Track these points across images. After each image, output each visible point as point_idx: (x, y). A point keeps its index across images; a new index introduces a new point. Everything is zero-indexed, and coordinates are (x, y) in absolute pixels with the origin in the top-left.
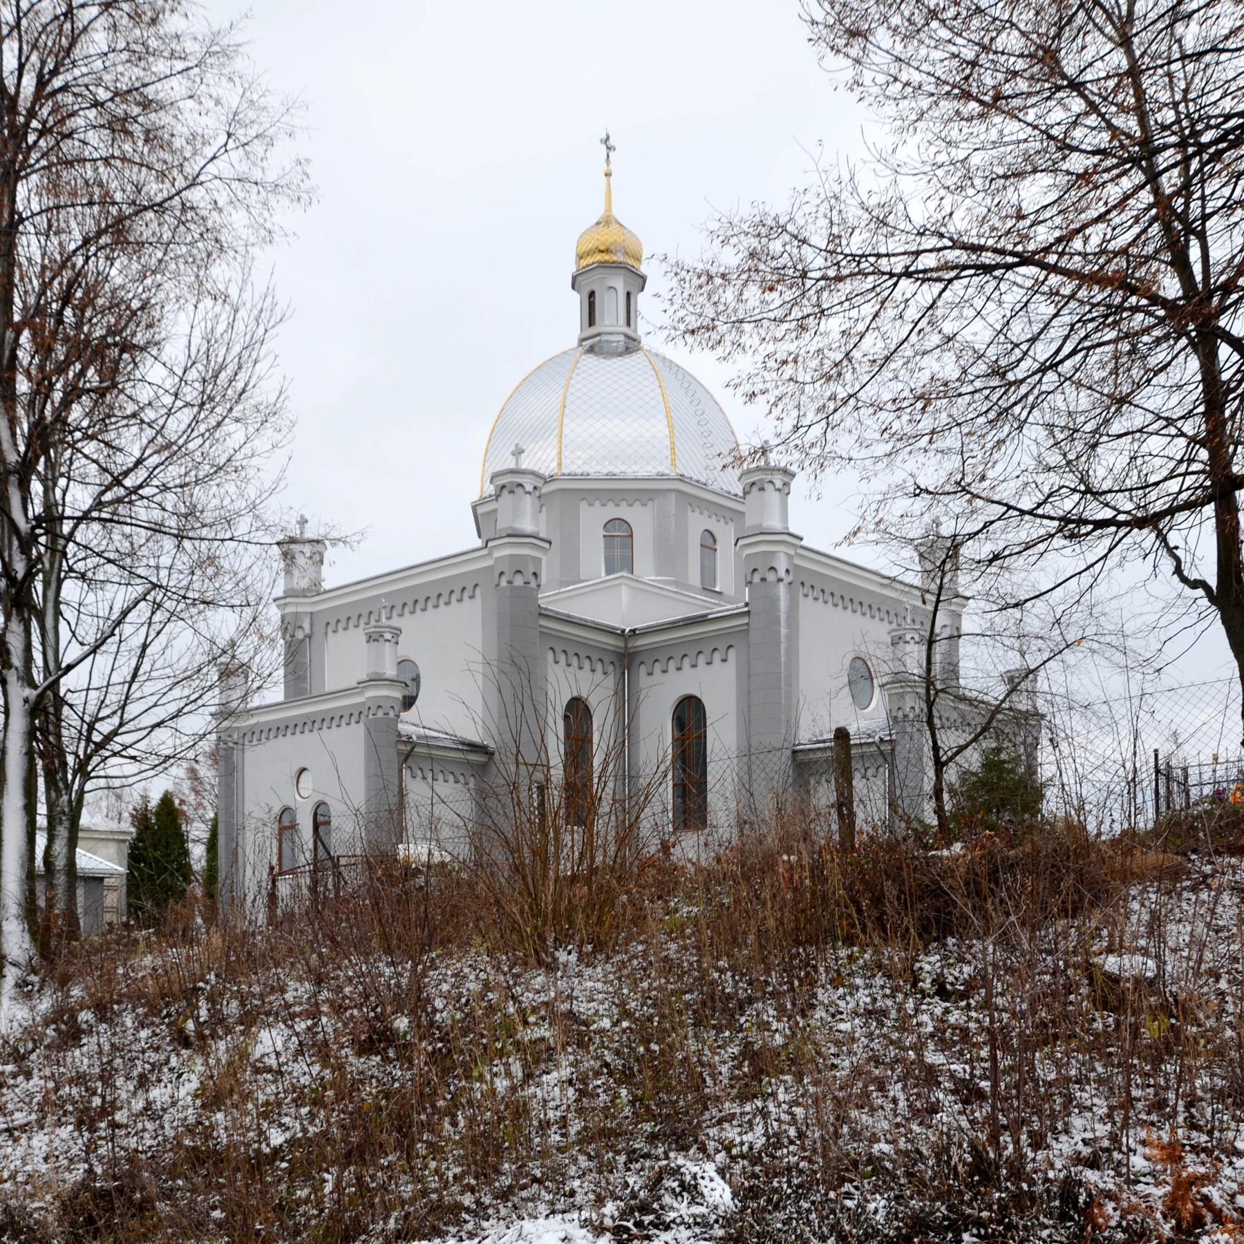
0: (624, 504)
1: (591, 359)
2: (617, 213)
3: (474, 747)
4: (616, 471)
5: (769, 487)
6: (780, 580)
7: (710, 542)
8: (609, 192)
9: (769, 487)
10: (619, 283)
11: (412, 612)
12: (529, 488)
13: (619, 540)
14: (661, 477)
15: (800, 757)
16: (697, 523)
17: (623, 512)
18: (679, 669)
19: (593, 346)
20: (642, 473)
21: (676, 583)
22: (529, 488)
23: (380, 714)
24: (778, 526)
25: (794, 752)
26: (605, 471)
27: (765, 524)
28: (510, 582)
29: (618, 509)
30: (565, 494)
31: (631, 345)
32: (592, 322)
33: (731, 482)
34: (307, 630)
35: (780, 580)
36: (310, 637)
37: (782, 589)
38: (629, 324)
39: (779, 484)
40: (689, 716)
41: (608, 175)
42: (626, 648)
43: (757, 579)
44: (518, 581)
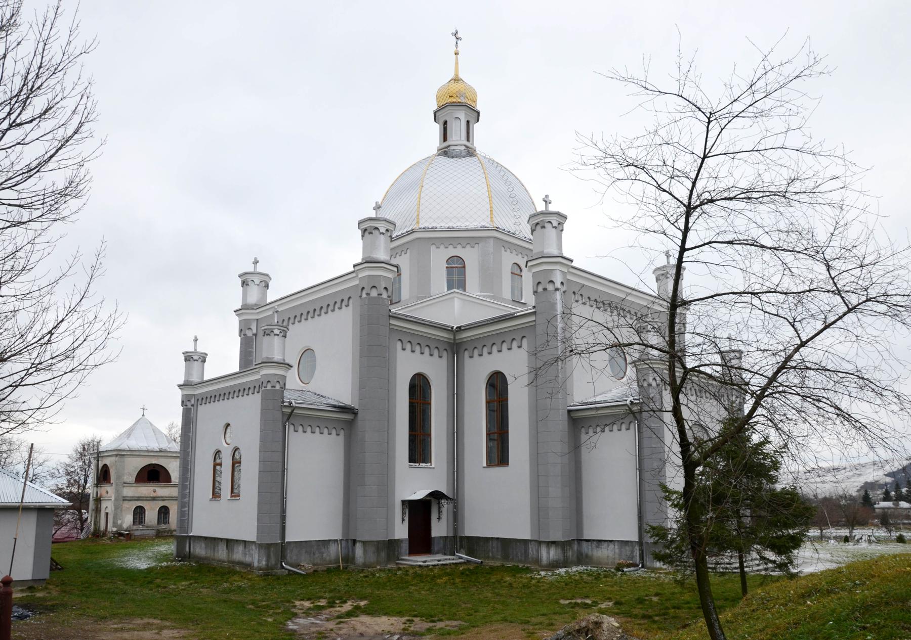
0: (459, 246)
1: (443, 159)
2: (461, 76)
3: (344, 409)
4: (455, 226)
5: (548, 226)
6: (557, 289)
7: (518, 271)
8: (457, 63)
9: (548, 226)
10: (462, 115)
11: (313, 317)
12: (383, 230)
13: (456, 273)
14: (484, 229)
15: (573, 415)
16: (509, 259)
17: (459, 252)
18: (490, 353)
19: (445, 152)
20: (472, 226)
21: (493, 297)
22: (383, 230)
23: (269, 387)
24: (556, 253)
25: (569, 411)
26: (447, 226)
27: (546, 251)
28: (368, 294)
29: (460, 253)
30: (422, 240)
31: (470, 152)
32: (445, 139)
33: (525, 230)
34: (255, 331)
35: (557, 289)
36: (256, 335)
37: (558, 295)
38: (468, 140)
39: (555, 224)
40: (497, 385)
41: (456, 54)
42: (455, 339)
43: (540, 289)
44: (374, 293)
